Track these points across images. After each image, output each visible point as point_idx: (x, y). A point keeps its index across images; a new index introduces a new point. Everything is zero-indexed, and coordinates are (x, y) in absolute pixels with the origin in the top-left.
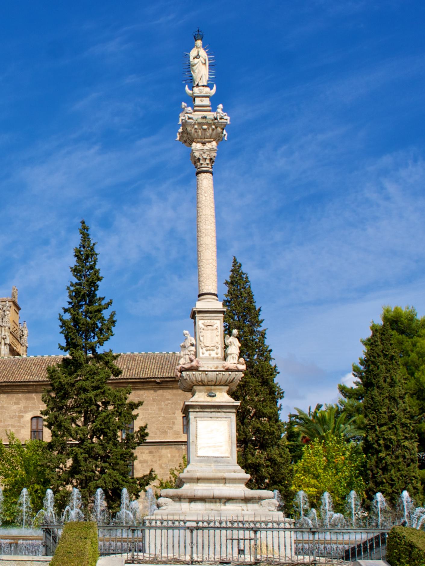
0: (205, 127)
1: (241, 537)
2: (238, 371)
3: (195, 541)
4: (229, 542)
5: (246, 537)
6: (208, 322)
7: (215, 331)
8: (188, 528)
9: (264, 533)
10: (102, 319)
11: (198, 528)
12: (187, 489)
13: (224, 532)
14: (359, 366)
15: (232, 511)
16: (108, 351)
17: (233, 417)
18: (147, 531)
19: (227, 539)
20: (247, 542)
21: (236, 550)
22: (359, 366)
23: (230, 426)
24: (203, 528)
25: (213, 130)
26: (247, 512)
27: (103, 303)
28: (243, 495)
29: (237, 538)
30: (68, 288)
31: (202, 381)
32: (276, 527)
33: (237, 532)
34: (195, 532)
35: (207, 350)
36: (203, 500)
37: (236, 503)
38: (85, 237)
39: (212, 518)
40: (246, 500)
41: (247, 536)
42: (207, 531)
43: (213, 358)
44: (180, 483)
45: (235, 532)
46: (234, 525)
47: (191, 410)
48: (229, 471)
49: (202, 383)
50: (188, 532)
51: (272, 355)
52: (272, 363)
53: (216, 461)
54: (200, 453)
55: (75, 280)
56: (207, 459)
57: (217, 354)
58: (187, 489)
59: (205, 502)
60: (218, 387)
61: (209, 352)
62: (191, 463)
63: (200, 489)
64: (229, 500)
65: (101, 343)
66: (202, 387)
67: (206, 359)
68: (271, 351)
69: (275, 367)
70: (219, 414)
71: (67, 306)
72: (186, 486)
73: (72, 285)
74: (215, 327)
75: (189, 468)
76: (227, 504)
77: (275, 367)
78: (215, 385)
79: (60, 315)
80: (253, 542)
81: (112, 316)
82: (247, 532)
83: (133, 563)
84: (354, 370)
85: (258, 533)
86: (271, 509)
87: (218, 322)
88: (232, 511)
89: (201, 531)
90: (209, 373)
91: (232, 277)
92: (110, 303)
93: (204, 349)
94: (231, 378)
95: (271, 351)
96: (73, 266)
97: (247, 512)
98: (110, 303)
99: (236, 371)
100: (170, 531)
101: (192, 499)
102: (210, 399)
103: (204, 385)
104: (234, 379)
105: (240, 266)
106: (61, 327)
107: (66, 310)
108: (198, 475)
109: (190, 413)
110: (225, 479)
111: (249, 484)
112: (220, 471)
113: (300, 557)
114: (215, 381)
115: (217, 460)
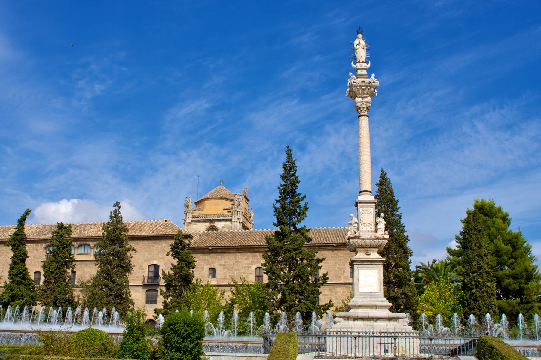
0: (364, 88)
1: (386, 342)
2: (384, 239)
3: (357, 345)
4: (379, 345)
6: (366, 209)
7: (370, 215)
8: (353, 336)
9: (400, 340)
10: (300, 207)
11: (359, 337)
12: (353, 312)
13: (375, 339)
14: (460, 236)
15: (380, 326)
16: (303, 226)
17: (381, 267)
18: (328, 338)
20: (390, 345)
21: (383, 350)
22: (460, 236)
23: (379, 273)
24: (370, 337)
25: (369, 89)
26: (391, 326)
27: (301, 197)
30: (279, 188)
31: (362, 245)
32: (407, 336)
34: (357, 339)
36: (362, 319)
38: (289, 156)
39: (368, 330)
40: (389, 319)
41: (390, 342)
43: (369, 231)
44: (348, 309)
46: (382, 335)
48: (379, 301)
49: (362, 247)
50: (353, 339)
51: (405, 229)
53: (370, 295)
54: (361, 290)
55: (283, 183)
56: (365, 294)
58: (353, 312)
63: (361, 312)
64: (378, 319)
65: (299, 222)
66: (362, 249)
67: (364, 231)
68: (404, 226)
69: (407, 236)
70: (372, 266)
71: (278, 199)
73: (281, 186)
74: (370, 212)
75: (354, 299)
77: (407, 236)
80: (393, 345)
81: (306, 205)
82: (390, 339)
83: (319, 358)
84: (456, 239)
85: (397, 340)
86: (405, 324)
88: (380, 326)
91: (380, 181)
92: (305, 197)
94: (380, 243)
95: (404, 226)
96: (281, 174)
97: (391, 326)
98: (305, 197)
100: (342, 338)
101: (356, 319)
102: (366, 256)
103: (363, 248)
105: (386, 174)
106: (274, 212)
107: (277, 202)
110: (376, 306)
111: (391, 309)
112: (373, 301)
113: (423, 355)
115: (371, 294)
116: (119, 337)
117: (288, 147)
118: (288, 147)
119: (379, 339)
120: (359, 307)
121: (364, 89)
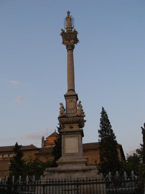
1: (67, 189)
5: (66, 189)
8: (42, 185)
12: (60, 167)
18: (36, 187)
19: (62, 191)
25: (72, 36)
28: (82, 168)
29: (64, 189)
33: (64, 186)
35: (70, 110)
37: (80, 172)
42: (55, 186)
43: (72, 113)
44: (56, 165)
45: (67, 186)
47: (62, 134)
48: (78, 159)
50: (42, 187)
52: (85, 118)
53: (72, 155)
57: (74, 111)
58: (60, 167)
59: (66, 172)
60: (74, 124)
61: (70, 111)
62: (62, 157)
64: (76, 171)
66: (67, 125)
72: (59, 167)
74: (73, 101)
76: (76, 173)
78: (73, 123)
79: (62, 30)
80: (76, 191)
85: (79, 186)
87: (74, 99)
89: (55, 186)
90: (69, 118)
93: (69, 110)
94: (78, 120)
99: (80, 116)
101: (60, 172)
102: (70, 129)
103: (68, 124)
104: (80, 119)
108: (64, 161)
109: (62, 136)
110: (76, 162)
114: (72, 121)
115: (72, 154)
116: (67, 101)
117: (69, 13)
118: (69, 13)
119: (64, 186)
120: (64, 163)
121: (69, 36)
